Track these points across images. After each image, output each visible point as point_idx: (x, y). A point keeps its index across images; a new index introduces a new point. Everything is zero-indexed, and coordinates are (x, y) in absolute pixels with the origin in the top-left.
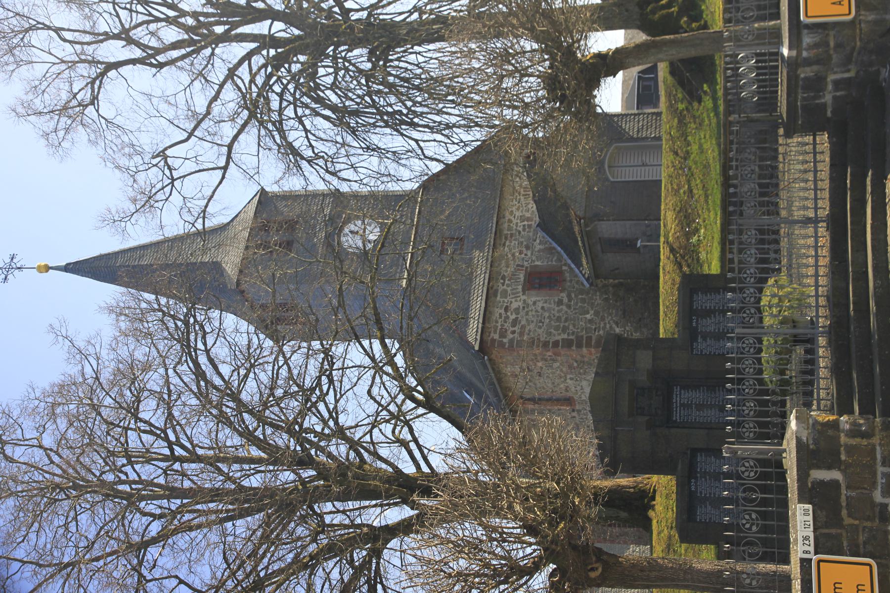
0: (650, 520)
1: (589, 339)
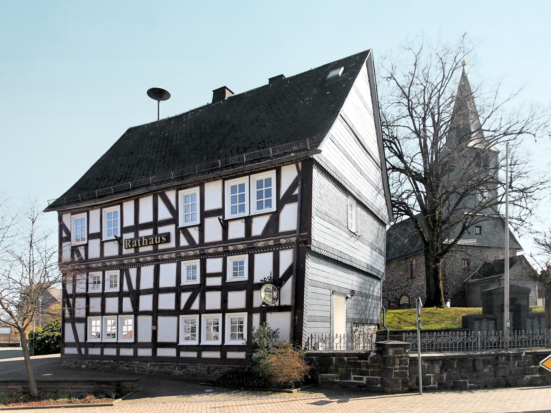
0: (433, 307)
1: (446, 283)
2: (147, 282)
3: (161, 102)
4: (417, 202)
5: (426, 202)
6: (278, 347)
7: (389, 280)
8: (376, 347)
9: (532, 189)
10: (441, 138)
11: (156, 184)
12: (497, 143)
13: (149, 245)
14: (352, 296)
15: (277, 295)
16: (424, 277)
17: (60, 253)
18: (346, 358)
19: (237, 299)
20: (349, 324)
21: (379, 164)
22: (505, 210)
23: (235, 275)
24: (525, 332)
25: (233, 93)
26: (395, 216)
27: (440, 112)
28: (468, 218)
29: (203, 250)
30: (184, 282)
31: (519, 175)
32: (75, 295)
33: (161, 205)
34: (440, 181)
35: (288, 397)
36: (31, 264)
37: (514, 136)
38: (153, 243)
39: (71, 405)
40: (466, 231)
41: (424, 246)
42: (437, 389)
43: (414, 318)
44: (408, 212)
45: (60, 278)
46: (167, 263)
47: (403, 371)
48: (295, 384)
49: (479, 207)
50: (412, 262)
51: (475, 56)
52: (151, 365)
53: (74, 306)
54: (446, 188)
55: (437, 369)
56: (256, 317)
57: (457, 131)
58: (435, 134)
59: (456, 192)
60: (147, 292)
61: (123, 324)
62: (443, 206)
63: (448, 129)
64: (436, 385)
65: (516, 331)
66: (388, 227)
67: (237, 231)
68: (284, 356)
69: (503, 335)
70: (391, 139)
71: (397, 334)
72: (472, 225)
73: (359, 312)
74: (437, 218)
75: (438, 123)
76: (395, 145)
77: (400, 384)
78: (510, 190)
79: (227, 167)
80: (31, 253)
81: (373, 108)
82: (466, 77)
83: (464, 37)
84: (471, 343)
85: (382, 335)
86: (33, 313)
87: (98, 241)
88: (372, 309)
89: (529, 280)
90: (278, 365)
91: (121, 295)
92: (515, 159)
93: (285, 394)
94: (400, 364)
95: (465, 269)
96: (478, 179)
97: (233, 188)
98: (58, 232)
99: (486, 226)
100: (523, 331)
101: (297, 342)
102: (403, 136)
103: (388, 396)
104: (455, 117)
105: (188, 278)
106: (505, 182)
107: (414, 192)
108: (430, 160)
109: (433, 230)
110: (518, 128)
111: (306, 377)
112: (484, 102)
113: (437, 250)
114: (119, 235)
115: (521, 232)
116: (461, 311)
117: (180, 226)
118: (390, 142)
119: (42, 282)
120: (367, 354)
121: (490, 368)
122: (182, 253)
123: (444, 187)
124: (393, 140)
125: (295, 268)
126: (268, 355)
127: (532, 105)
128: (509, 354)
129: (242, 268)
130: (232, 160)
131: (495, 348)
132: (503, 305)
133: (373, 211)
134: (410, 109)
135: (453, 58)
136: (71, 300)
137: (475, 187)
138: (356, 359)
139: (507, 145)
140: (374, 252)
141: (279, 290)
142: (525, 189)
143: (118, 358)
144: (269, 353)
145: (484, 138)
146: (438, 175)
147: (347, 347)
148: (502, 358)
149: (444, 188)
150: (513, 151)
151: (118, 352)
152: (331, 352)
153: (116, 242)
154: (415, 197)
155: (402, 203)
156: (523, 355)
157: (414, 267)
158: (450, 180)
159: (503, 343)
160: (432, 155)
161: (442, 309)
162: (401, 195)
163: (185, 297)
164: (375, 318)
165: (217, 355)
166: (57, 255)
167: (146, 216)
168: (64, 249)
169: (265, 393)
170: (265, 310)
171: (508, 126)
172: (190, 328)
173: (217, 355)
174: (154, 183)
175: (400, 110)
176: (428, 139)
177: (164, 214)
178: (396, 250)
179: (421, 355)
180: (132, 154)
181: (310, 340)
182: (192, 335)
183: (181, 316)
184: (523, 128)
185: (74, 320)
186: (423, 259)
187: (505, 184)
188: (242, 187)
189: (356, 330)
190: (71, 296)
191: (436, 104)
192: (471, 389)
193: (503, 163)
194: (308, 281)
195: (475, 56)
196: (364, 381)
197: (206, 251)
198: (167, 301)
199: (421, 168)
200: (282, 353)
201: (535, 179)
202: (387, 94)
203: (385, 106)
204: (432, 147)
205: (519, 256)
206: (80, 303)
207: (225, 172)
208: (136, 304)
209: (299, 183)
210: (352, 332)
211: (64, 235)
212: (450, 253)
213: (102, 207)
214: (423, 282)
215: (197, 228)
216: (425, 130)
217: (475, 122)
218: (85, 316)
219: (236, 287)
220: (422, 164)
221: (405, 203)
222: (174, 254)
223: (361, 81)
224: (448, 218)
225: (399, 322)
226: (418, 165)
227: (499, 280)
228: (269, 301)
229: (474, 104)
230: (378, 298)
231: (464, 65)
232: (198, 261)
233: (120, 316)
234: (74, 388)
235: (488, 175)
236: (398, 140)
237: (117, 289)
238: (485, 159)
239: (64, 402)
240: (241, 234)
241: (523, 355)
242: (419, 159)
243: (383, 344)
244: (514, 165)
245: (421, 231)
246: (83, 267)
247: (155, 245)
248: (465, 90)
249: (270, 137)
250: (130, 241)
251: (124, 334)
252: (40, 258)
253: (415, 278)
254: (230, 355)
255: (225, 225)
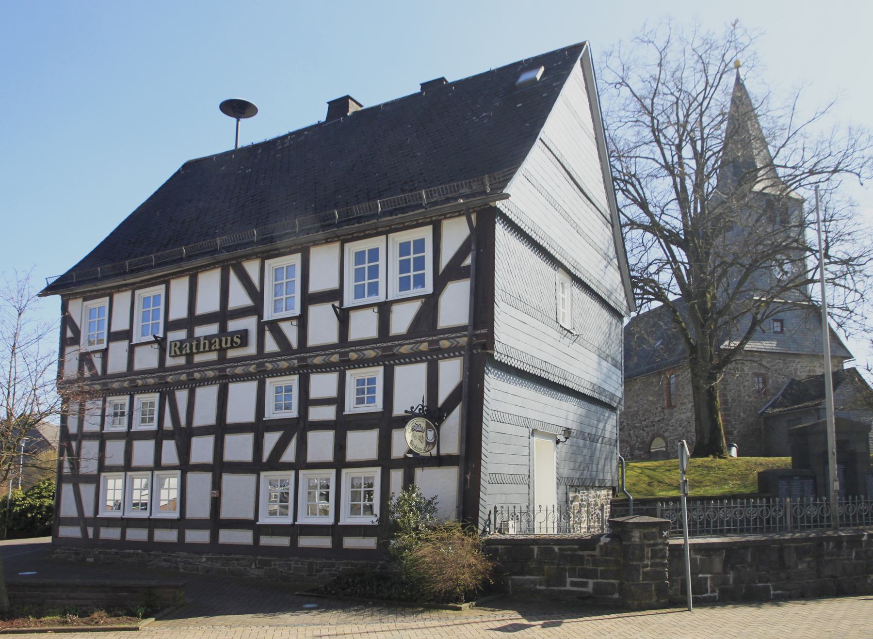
0: (707, 456)
1: (729, 415)
2: (205, 412)
3: (243, 122)
4: (674, 279)
5: (688, 278)
6: (434, 529)
7: (631, 410)
8: (610, 527)
9: (862, 260)
10: (708, 177)
11: (228, 249)
12: (800, 186)
13: (210, 350)
14: (567, 438)
15: (435, 436)
16: (690, 405)
17: (61, 364)
18: (556, 548)
19: (363, 444)
20: (562, 488)
21: (608, 217)
22: (820, 293)
23: (360, 401)
24: (866, 498)
25: (361, 106)
26: (639, 302)
27: (705, 136)
28: (759, 306)
29: (305, 359)
30: (270, 414)
31: (839, 238)
32: (82, 436)
33: (235, 283)
34: (711, 244)
35: (453, 617)
36: (12, 383)
37: (826, 175)
38: (218, 347)
39: (66, 627)
40: (758, 328)
41: (688, 352)
42: (719, 601)
43: (676, 476)
44: (660, 295)
45: (58, 407)
46: (241, 381)
47: (658, 569)
48: (466, 594)
49: (778, 289)
50: (669, 379)
51: (755, 54)
52: (207, 559)
53: (79, 454)
54: (721, 257)
55: (718, 565)
56: (397, 476)
57: (735, 167)
58: (699, 171)
59: (738, 263)
60: (204, 431)
61: (161, 486)
62: (718, 285)
63: (719, 163)
64: (716, 594)
65: (850, 497)
66: (626, 321)
67: (364, 326)
68: (445, 544)
69: (828, 504)
70: (627, 178)
71: (646, 505)
72: (767, 317)
73: (580, 466)
74: (709, 305)
75: (702, 154)
76: (634, 186)
77: (654, 593)
78: (827, 261)
79: (349, 222)
80: (13, 365)
81: (595, 129)
82: (743, 85)
83: (734, 25)
84: (774, 519)
85: (619, 506)
86: (10, 465)
87: (125, 344)
88: (602, 462)
89: (866, 410)
90: (435, 560)
91: (159, 436)
92: (830, 212)
93: (448, 611)
94: (653, 557)
95: (759, 392)
96: (773, 243)
97: (359, 257)
98: (59, 330)
99: (792, 319)
100: (862, 497)
101: (469, 520)
102: (646, 172)
103: (632, 614)
104: (730, 145)
105: (278, 408)
106: (817, 248)
107: (668, 262)
108: (692, 211)
109: (703, 326)
110: (831, 163)
111: (485, 582)
112: (773, 122)
113: (711, 360)
114: (161, 335)
115: (849, 330)
116: (755, 464)
117: (266, 318)
118: (626, 182)
119: (28, 413)
120: (596, 539)
121: (809, 562)
122: (267, 364)
123: (717, 254)
124: (631, 179)
125: (465, 390)
126: (417, 543)
127: (850, 129)
128: (840, 536)
129: (372, 391)
130: (357, 210)
131: (816, 527)
132: (826, 452)
133: (600, 293)
134: (656, 131)
135: (720, 57)
136: (74, 444)
137: (769, 255)
138: (575, 550)
139: (816, 190)
140: (604, 363)
141: (438, 428)
142: (851, 259)
143: (150, 545)
144: (419, 539)
145: (777, 177)
146: (707, 235)
147: (559, 527)
148: (828, 544)
149: (718, 256)
150: (827, 199)
151: (151, 535)
152: (529, 537)
153: (156, 346)
154: (671, 271)
155: (649, 281)
156: (865, 538)
157: (673, 387)
158: (726, 244)
159: (828, 518)
160: (696, 203)
161: (723, 461)
162: (647, 268)
163: (271, 439)
164: (608, 477)
165: (325, 542)
166: (55, 367)
167: (208, 303)
168: (67, 357)
169: (411, 610)
170: (412, 463)
171: (815, 160)
172: (278, 494)
173: (325, 542)
174: (224, 248)
175: (638, 133)
176: (687, 177)
177: (239, 298)
178: (639, 358)
179: (689, 541)
180: (190, 201)
181: (492, 517)
182: (281, 506)
183: (263, 474)
184: (839, 163)
185: (77, 479)
186: (688, 375)
187: (817, 251)
188: (374, 254)
189: (575, 498)
190: (74, 437)
191: (698, 124)
192: (777, 600)
193: (812, 217)
194: (490, 412)
195: (755, 54)
196: (590, 589)
197: (309, 361)
198: (238, 448)
199: (678, 224)
200: (443, 539)
201: (865, 244)
202: (617, 109)
203: (615, 126)
204: (694, 191)
205: (848, 370)
206: (90, 448)
207: (346, 228)
208: (184, 451)
209: (473, 247)
210: (567, 501)
211: (69, 334)
212: (733, 364)
213: (134, 287)
214: (689, 414)
215: (295, 322)
216: (681, 165)
217: (762, 154)
218: (96, 472)
219: (362, 422)
220: (680, 217)
221: (653, 281)
222: (254, 366)
223: (574, 85)
224: (727, 307)
225: (650, 484)
226: (673, 220)
227: (818, 410)
228: (420, 448)
229: (759, 125)
230: (613, 442)
231: (737, 66)
232: (296, 378)
233: (156, 473)
234: (73, 598)
235: (789, 237)
236: (638, 180)
237: (153, 426)
238: (782, 211)
239: (53, 623)
240: (372, 332)
241: (865, 538)
242: (674, 208)
243: (622, 522)
244: (830, 221)
245: (682, 328)
246: (98, 387)
247: (222, 351)
248: (743, 104)
249: (422, 174)
250: (178, 344)
251: (162, 503)
252: (27, 373)
253: (675, 406)
254: (350, 542)
255: (343, 317)
